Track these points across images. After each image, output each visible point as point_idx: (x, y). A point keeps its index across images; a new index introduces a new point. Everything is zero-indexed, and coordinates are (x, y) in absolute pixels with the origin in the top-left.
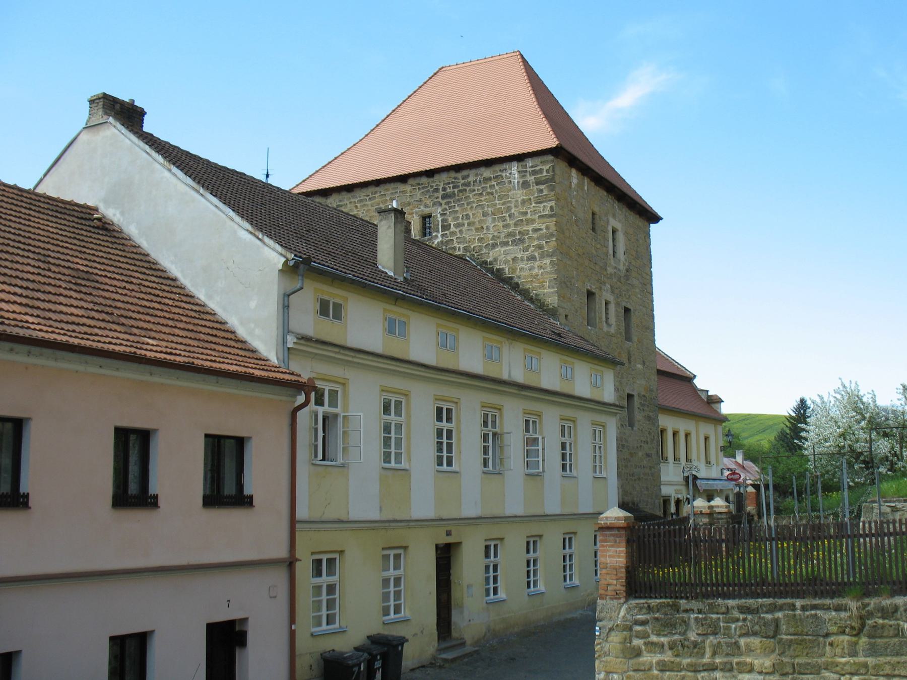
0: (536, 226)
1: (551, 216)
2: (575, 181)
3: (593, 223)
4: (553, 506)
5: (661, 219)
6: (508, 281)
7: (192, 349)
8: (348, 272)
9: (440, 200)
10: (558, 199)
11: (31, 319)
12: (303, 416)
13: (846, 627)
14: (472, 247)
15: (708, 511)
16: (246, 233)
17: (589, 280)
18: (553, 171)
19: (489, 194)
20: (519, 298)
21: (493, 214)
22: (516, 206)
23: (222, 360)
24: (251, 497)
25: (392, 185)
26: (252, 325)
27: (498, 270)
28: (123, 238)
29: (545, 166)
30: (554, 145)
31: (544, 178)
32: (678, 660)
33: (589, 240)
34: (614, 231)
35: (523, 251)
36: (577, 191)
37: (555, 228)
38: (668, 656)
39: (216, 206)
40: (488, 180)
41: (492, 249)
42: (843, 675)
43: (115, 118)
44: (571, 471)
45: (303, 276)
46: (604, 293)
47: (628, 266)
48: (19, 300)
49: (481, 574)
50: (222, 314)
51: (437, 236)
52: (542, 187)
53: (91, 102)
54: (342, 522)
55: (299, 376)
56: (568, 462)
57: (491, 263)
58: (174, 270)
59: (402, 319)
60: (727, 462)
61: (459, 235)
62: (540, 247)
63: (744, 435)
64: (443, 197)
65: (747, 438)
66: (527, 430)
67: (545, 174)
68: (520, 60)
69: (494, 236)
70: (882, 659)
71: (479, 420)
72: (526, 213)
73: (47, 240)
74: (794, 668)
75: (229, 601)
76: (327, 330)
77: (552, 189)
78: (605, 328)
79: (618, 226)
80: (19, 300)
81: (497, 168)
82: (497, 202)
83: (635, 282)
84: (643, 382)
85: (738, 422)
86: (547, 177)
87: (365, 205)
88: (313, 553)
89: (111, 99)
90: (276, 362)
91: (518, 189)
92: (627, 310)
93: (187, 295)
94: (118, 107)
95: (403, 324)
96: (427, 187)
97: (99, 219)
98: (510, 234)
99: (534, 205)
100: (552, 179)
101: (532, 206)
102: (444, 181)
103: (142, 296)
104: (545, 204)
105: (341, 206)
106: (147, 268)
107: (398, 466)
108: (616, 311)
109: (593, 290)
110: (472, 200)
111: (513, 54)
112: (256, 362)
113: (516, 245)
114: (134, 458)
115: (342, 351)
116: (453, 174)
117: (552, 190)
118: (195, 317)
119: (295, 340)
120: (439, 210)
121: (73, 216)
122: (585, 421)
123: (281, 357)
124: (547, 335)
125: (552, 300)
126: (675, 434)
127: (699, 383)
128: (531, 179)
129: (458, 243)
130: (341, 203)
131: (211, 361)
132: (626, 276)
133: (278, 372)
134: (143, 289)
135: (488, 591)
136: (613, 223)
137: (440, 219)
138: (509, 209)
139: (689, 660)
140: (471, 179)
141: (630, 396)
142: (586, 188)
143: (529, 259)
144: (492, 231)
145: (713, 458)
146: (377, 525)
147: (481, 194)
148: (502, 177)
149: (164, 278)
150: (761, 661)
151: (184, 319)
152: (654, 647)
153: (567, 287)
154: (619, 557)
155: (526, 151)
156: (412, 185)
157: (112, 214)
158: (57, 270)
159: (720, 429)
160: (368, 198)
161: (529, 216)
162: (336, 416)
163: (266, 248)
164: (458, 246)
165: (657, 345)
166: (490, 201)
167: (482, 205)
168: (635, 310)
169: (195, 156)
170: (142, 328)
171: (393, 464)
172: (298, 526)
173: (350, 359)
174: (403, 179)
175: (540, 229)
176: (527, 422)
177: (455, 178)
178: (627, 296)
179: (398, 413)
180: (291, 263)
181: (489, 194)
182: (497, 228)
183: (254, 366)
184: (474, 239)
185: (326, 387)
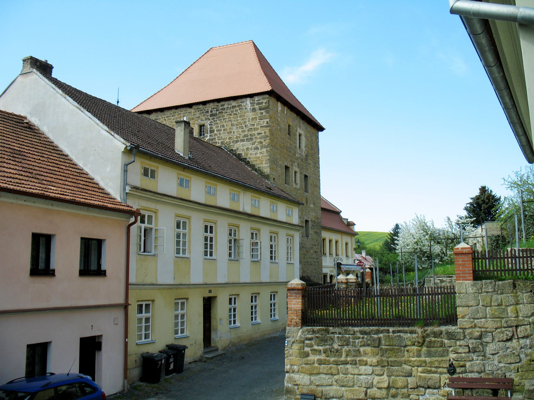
0: (259, 131)
1: (267, 127)
2: (280, 108)
3: (289, 131)
4: (265, 278)
5: (325, 129)
6: (244, 160)
8: (159, 153)
9: (209, 117)
10: (271, 118)
12: (133, 228)
15: (346, 281)
17: (286, 160)
19: (235, 114)
20: (249, 169)
21: (237, 125)
23: (90, 198)
24: (105, 271)
26: (107, 181)
27: (239, 154)
29: (264, 100)
30: (269, 90)
31: (264, 107)
32: (328, 358)
33: (287, 140)
34: (300, 135)
36: (281, 114)
38: (323, 357)
39: (90, 117)
42: (414, 367)
43: (37, 69)
44: (275, 259)
45: (135, 155)
46: (294, 167)
47: (307, 153)
50: (92, 174)
51: (207, 136)
52: (262, 111)
55: (132, 207)
56: (274, 255)
57: (235, 151)
58: (66, 150)
61: (218, 136)
62: (261, 143)
63: (366, 242)
64: (211, 116)
66: (252, 238)
67: (264, 104)
68: (253, 45)
71: (227, 232)
72: (254, 125)
75: (92, 326)
77: (268, 112)
78: (294, 186)
79: (302, 132)
81: (239, 101)
82: (239, 119)
83: (310, 162)
84: (314, 214)
85: (364, 235)
87: (170, 119)
88: (138, 301)
89: (35, 59)
90: (120, 200)
91: (250, 112)
92: (306, 176)
93: (73, 164)
94: (38, 64)
95: (188, 181)
98: (245, 136)
99: (258, 120)
100: (267, 108)
101: (257, 121)
102: (211, 107)
104: (264, 120)
105: (157, 119)
107: (184, 256)
108: (300, 176)
110: (226, 117)
111: (249, 42)
116: (216, 104)
117: (268, 113)
118: (77, 176)
119: (130, 189)
120: (209, 122)
122: (283, 234)
123: (122, 197)
124: (264, 188)
127: (343, 215)
128: (257, 107)
130: (157, 118)
132: (306, 158)
134: (50, 160)
137: (209, 127)
138: (245, 122)
140: (225, 106)
141: (307, 221)
142: (285, 112)
143: (255, 149)
144: (236, 134)
145: (350, 255)
147: (231, 114)
150: (371, 359)
152: (315, 351)
154: (298, 304)
156: (195, 109)
157: (34, 120)
159: (354, 239)
160: (171, 115)
161: (255, 126)
162: (151, 229)
163: (116, 140)
164: (218, 141)
166: (235, 118)
169: (80, 91)
171: (181, 255)
172: (130, 286)
173: (159, 199)
174: (190, 106)
175: (261, 133)
176: (252, 234)
177: (217, 106)
179: (184, 228)
180: (129, 148)
181: (235, 114)
184: (227, 138)
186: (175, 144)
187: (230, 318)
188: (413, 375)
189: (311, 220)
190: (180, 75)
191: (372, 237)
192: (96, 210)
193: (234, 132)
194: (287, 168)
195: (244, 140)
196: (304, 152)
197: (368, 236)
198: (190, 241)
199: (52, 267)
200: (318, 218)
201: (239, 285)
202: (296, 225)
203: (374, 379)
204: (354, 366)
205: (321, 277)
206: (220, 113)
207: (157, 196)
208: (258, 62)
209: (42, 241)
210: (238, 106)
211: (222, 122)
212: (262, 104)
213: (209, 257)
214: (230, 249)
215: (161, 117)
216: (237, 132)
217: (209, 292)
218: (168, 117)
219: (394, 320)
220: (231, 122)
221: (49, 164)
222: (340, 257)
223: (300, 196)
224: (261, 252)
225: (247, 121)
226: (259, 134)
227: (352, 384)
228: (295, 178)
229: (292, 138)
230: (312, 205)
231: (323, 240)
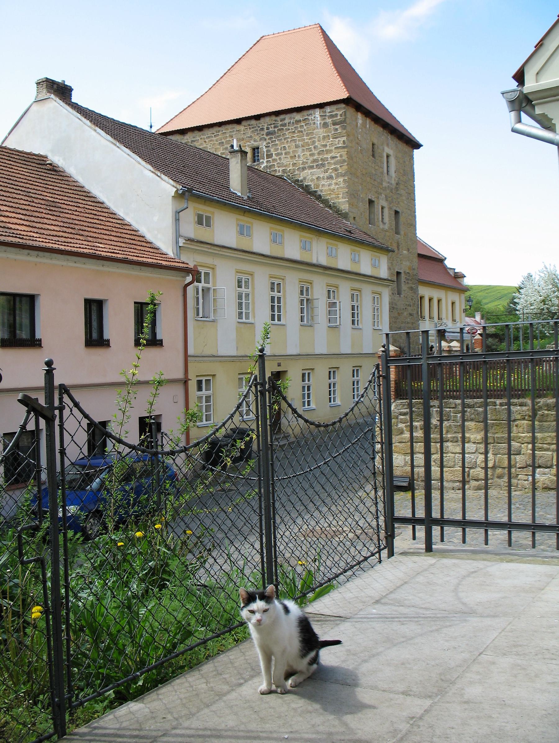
0: (333, 154)
1: (344, 148)
2: (360, 122)
3: (373, 151)
4: (346, 349)
5: (422, 146)
6: (313, 194)
7: (124, 249)
8: (214, 195)
9: (265, 136)
10: (348, 136)
11: (35, 235)
12: (190, 289)
13: (526, 416)
15: (448, 349)
16: (149, 172)
18: (345, 115)
19: (299, 132)
20: (321, 205)
21: (303, 146)
22: (319, 141)
23: (142, 255)
24: (161, 341)
25: (230, 126)
26: (156, 232)
27: (307, 186)
28: (66, 176)
29: (339, 112)
30: (345, 97)
31: (338, 121)
33: (370, 164)
34: (388, 156)
36: (362, 129)
37: (346, 156)
39: (128, 155)
40: (298, 122)
42: (523, 444)
43: (56, 95)
44: (358, 325)
45: (187, 200)
46: (381, 201)
48: (25, 223)
49: (300, 392)
50: (135, 225)
51: (263, 162)
52: (337, 127)
53: (38, 84)
54: (214, 356)
55: (188, 264)
56: (356, 319)
57: (302, 181)
58: (102, 197)
59: (248, 225)
60: (468, 320)
62: (336, 170)
63: (484, 301)
64: (267, 134)
65: (487, 304)
66: (329, 297)
67: (339, 117)
68: (320, 31)
70: (546, 434)
71: (298, 291)
72: (326, 146)
73: (26, 181)
74: (494, 440)
76: (202, 233)
77: (344, 128)
78: (381, 226)
79: (391, 152)
80: (25, 223)
81: (305, 113)
83: (402, 192)
84: (408, 264)
85: (481, 291)
87: (211, 141)
88: (197, 376)
90: (172, 255)
91: (320, 128)
92: (397, 213)
93: (112, 213)
94: (55, 86)
95: (249, 228)
97: (50, 164)
98: (315, 161)
99: (331, 139)
100: (344, 121)
103: (87, 215)
105: (194, 141)
106: (85, 196)
107: (247, 321)
108: (389, 213)
109: (373, 199)
111: (314, 26)
112: (161, 256)
114: (94, 317)
115: (212, 247)
116: (274, 118)
117: (345, 129)
118: (120, 228)
119: (184, 241)
120: (265, 143)
121: (34, 163)
122: (367, 291)
123: (175, 252)
124: (342, 232)
125: (344, 207)
126: (430, 300)
127: (449, 263)
128: (329, 121)
129: (278, 167)
131: (136, 256)
132: (396, 188)
133: (175, 262)
134: (87, 211)
135: (304, 402)
136: (388, 150)
137: (265, 150)
138: (314, 142)
140: (287, 121)
141: (398, 273)
142: (368, 126)
143: (328, 178)
144: (302, 158)
145: (457, 318)
146: (235, 359)
147: (294, 132)
149: (96, 202)
150: (475, 436)
151: (114, 229)
153: (355, 197)
155: (325, 101)
158: (37, 202)
159: (463, 297)
160: (213, 135)
161: (328, 148)
162: (209, 289)
163: (163, 182)
168: (403, 212)
169: (105, 116)
170: (93, 237)
171: (244, 320)
172: (189, 358)
173: (217, 252)
174: (238, 121)
175: (336, 157)
176: (329, 291)
177: (276, 121)
179: (247, 286)
180: (180, 192)
181: (299, 132)
182: (306, 156)
183: (161, 259)
185: (202, 270)
186: (230, 181)
187: (304, 398)
188: (522, 453)
189: (405, 272)
190: (222, 77)
191: (494, 293)
192: (150, 269)
193: (299, 156)
194: (371, 202)
195: (313, 166)
196: (393, 179)
197: (487, 291)
198: (254, 303)
200: (414, 269)
201: (314, 356)
202: (385, 280)
203: (477, 458)
204: (455, 444)
205: (418, 348)
206: (279, 130)
207: (215, 248)
208: (328, 56)
209: (94, 308)
210: (303, 120)
211: (283, 143)
213: (276, 321)
214: (302, 312)
216: (303, 156)
217: (278, 366)
218: (209, 137)
219: (502, 391)
220: (296, 142)
221: (87, 215)
222: (444, 321)
223: (390, 239)
224: (340, 314)
225: (316, 140)
226: (333, 158)
227: (453, 463)
228: (382, 215)
229: (377, 161)
230: (405, 252)
231: (421, 298)
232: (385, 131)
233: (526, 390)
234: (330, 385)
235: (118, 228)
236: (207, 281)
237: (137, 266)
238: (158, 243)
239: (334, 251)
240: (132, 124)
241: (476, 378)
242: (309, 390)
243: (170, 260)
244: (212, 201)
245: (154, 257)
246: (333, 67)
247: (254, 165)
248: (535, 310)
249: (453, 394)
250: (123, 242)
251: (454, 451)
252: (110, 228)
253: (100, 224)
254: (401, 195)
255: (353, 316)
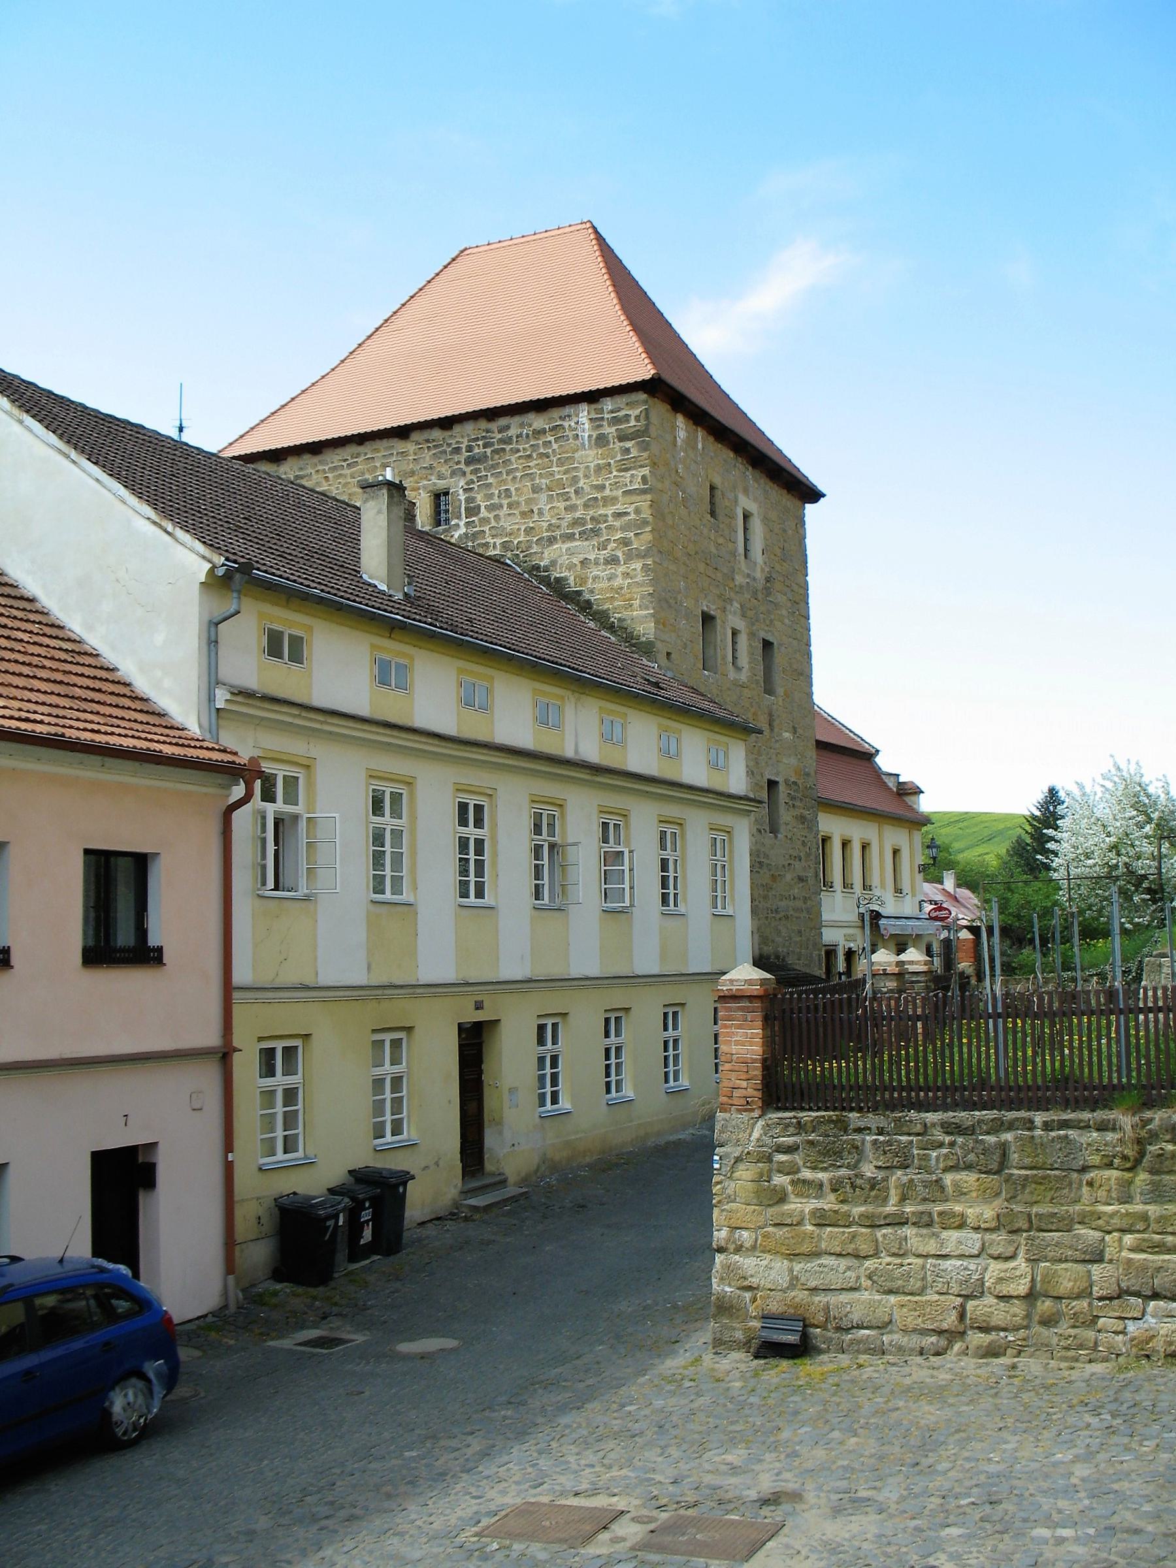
0: (619, 508)
1: (644, 492)
2: (682, 434)
3: (712, 503)
4: (647, 962)
5: (823, 495)
6: (574, 598)
9: (462, 466)
10: (654, 465)
12: (242, 819)
14: (516, 542)
15: (896, 970)
16: (147, 522)
18: (647, 418)
19: (542, 455)
20: (592, 625)
21: (549, 489)
22: (586, 476)
23: (110, 729)
24: (160, 950)
25: (385, 443)
27: (558, 580)
29: (634, 410)
30: (648, 377)
33: (705, 531)
34: (746, 516)
35: (599, 549)
36: (686, 451)
38: (828, 1203)
39: (97, 480)
41: (548, 546)
42: (1109, 1233)
45: (239, 592)
47: (770, 572)
50: (110, 656)
51: (457, 525)
52: (629, 444)
55: (236, 754)
56: (671, 891)
57: (546, 569)
59: (401, 661)
62: (625, 542)
63: (957, 845)
64: (469, 462)
65: (962, 851)
66: (605, 840)
67: (633, 423)
68: (592, 236)
69: (550, 525)
71: (527, 823)
72: (602, 488)
74: (1030, 1222)
77: (644, 447)
78: (732, 675)
79: (753, 507)
81: (555, 413)
83: (781, 599)
84: (793, 761)
86: (637, 428)
88: (260, 1039)
90: (198, 731)
91: (590, 448)
92: (767, 645)
93: (53, 626)
95: (403, 669)
96: (441, 445)
98: (576, 522)
99: (615, 473)
100: (644, 432)
105: (302, 477)
108: (750, 645)
110: (515, 466)
112: (167, 731)
113: (586, 539)
115: (304, 714)
116: (483, 424)
117: (645, 450)
118: (65, 661)
119: (228, 697)
120: (462, 483)
123: (206, 724)
125: (646, 629)
126: (845, 844)
127: (884, 762)
129: (493, 536)
131: (92, 731)
132: (766, 588)
133: (201, 748)
135: (542, 1097)
137: (462, 498)
138: (575, 480)
139: (863, 1209)
140: (513, 432)
141: (772, 784)
142: (700, 446)
143: (607, 562)
144: (547, 517)
145: (906, 885)
147: (530, 456)
148: (564, 428)
150: (978, 1210)
151: (47, 663)
159: (917, 837)
160: (345, 464)
161: (607, 492)
162: (296, 818)
163: (180, 547)
165: (816, 701)
167: (531, 474)
169: (63, 398)
171: (388, 896)
173: (318, 726)
174: (402, 433)
176: (605, 825)
177: (488, 431)
178: (768, 622)
179: (396, 813)
180: (221, 572)
181: (542, 455)
182: (556, 511)
183: (162, 738)
184: (519, 529)
185: (280, 772)
188: (1107, 1257)
189: (786, 781)
190: (369, 337)
193: (541, 513)
194: (707, 619)
196: (759, 570)
197: (961, 825)
199: (153, 941)
200: (808, 775)
202: (740, 798)
204: (924, 1231)
207: (312, 715)
210: (551, 430)
211: (504, 482)
212: (628, 421)
214: (538, 876)
215: (313, 471)
216: (549, 510)
217: (477, 1009)
219: (1048, 1088)
220: (533, 480)
225: (581, 474)
226: (619, 515)
227: (919, 1284)
228: (734, 650)
229: (721, 526)
230: (786, 735)
232: (740, 460)
233: (1114, 1087)
234: (607, 1051)
235: (59, 660)
236: (290, 798)
237: (93, 757)
238: (164, 702)
239: (618, 730)
240: (133, 421)
241: (970, 1044)
242: (554, 1064)
243: (186, 742)
244: (306, 597)
245: (143, 735)
246: (620, 313)
247: (437, 532)
248: (1097, 869)
249: (918, 1095)
250: (66, 696)
251: (923, 1250)
252: (35, 661)
253: (12, 650)
254: (777, 605)
255: (664, 885)
